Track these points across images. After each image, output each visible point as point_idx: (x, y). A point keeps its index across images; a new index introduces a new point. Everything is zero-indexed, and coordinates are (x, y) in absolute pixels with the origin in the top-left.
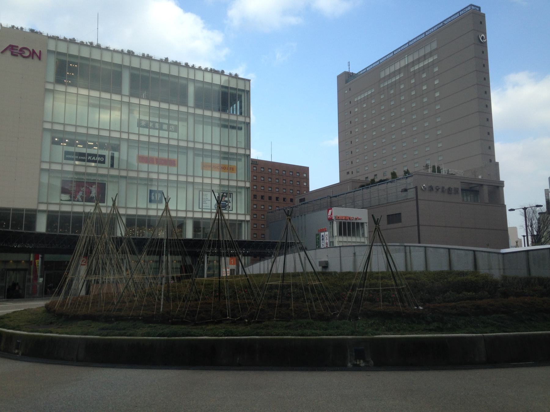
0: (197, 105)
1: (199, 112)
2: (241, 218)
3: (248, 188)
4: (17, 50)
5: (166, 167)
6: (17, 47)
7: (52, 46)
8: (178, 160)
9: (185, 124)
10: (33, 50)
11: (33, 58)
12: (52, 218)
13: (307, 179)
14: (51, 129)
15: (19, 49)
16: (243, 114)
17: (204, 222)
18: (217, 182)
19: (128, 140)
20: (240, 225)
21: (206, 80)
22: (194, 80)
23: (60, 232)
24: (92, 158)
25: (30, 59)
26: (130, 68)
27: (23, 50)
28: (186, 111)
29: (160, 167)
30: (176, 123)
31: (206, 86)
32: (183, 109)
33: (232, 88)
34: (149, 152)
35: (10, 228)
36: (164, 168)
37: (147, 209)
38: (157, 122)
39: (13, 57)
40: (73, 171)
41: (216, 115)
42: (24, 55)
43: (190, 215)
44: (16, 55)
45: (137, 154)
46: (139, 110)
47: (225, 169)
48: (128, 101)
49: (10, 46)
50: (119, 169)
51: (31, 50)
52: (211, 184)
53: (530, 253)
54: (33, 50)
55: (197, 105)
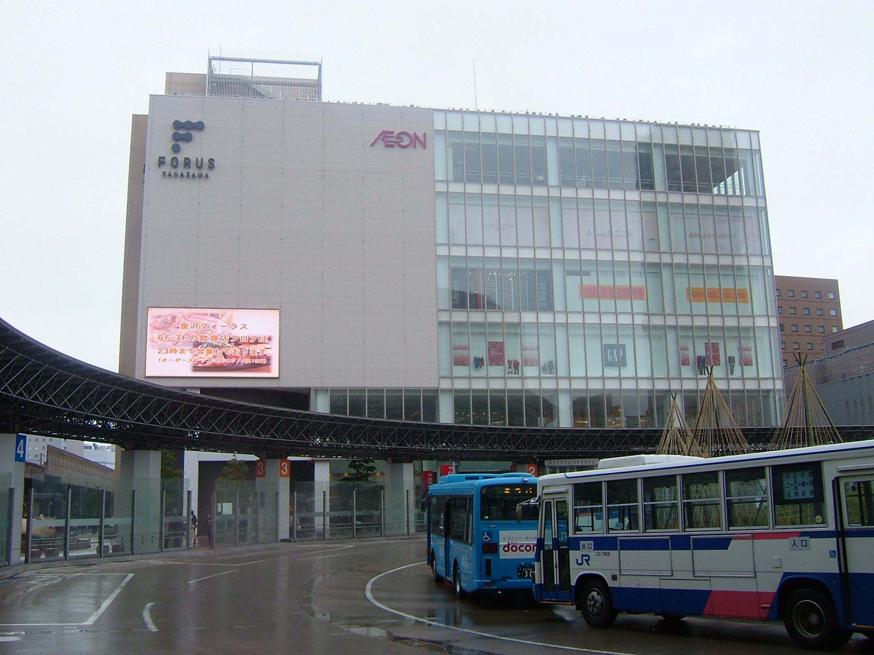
0: (673, 186)
1: (675, 198)
2: (767, 385)
5: (628, 302)
6: (392, 133)
7: (439, 125)
8: (647, 287)
11: (415, 147)
12: (461, 403)
13: (836, 303)
15: (395, 135)
17: (347, 390)
18: (640, 320)
19: (563, 261)
21: (533, 133)
22: (557, 137)
25: (411, 148)
26: (557, 139)
27: (401, 136)
28: (512, 193)
29: (619, 302)
31: (594, 147)
32: (540, 191)
33: (683, 147)
34: (632, 279)
37: (603, 378)
39: (388, 149)
41: (633, 195)
42: (401, 143)
44: (392, 146)
45: (580, 283)
46: (624, 209)
47: (729, 297)
48: (576, 196)
49: (384, 132)
51: (412, 136)
52: (617, 324)
54: (415, 133)
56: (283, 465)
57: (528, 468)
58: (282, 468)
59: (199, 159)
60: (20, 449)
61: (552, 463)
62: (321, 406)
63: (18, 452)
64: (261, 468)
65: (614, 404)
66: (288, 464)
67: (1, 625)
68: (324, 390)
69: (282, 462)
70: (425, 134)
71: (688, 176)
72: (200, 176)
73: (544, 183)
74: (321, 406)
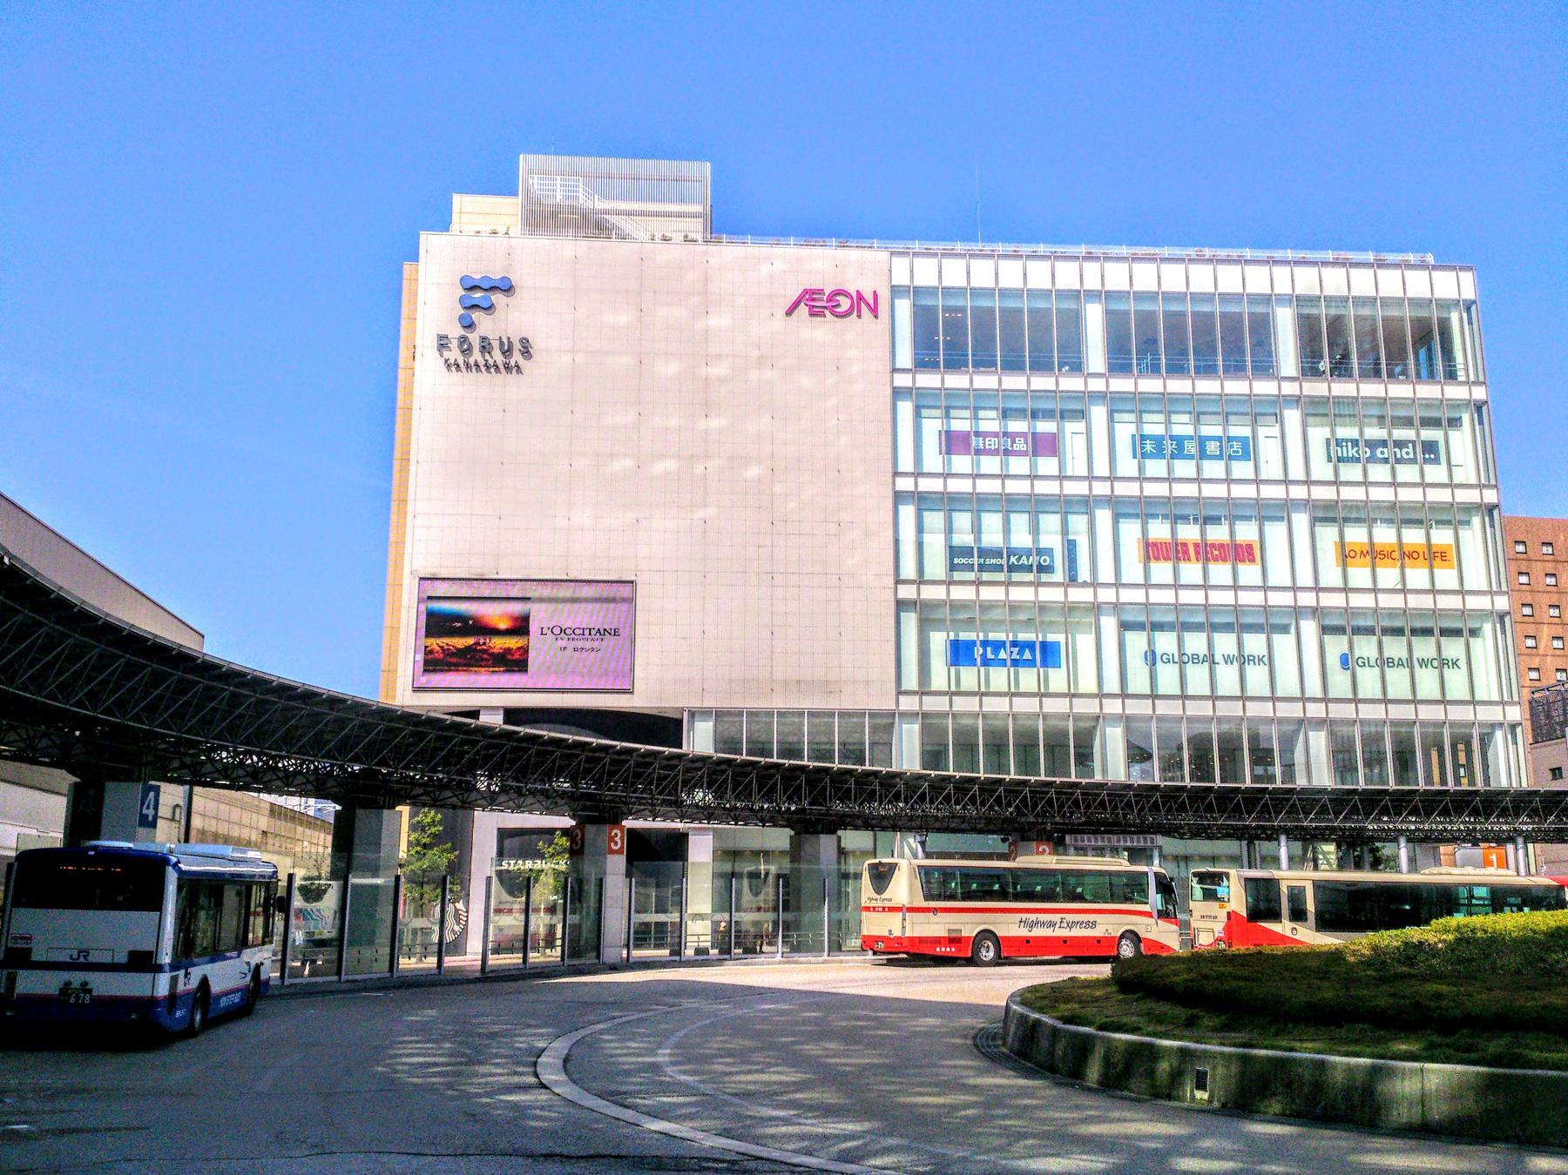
0: (1119, 363)
3: (1501, 617)
4: (822, 300)
6: (821, 292)
9: (1275, 431)
10: (858, 292)
11: (859, 316)
14: (942, 493)
16: (1461, 376)
20: (1486, 741)
23: (1255, 778)
24: (1018, 560)
27: (838, 298)
30: (1245, 431)
35: (951, 769)
36: (1220, 572)
38: (1191, 438)
40: (1064, 603)
42: (838, 310)
43: (1113, 707)
45: (1140, 536)
49: (806, 291)
50: (1094, 584)
51: (854, 295)
53: (886, 750)
55: (1119, 363)
56: (613, 834)
57: (1038, 848)
58: (612, 839)
59: (505, 340)
60: (148, 808)
61: (1135, 840)
62: (700, 741)
63: (145, 811)
64: (617, 839)
65: (1263, 745)
66: (622, 832)
67: (1563, 1074)
68: (705, 713)
69: (611, 830)
70: (875, 292)
71: (1149, 344)
72: (468, 366)
73: (1077, 367)
74: (700, 741)
